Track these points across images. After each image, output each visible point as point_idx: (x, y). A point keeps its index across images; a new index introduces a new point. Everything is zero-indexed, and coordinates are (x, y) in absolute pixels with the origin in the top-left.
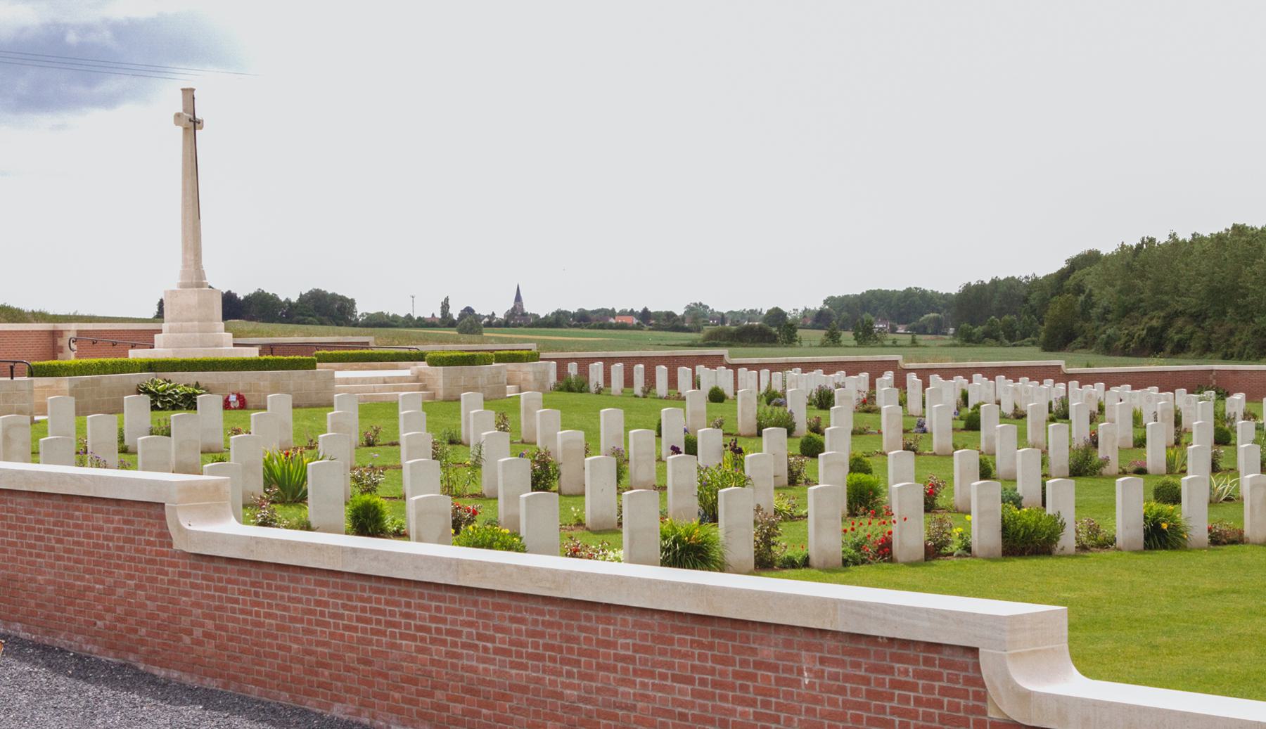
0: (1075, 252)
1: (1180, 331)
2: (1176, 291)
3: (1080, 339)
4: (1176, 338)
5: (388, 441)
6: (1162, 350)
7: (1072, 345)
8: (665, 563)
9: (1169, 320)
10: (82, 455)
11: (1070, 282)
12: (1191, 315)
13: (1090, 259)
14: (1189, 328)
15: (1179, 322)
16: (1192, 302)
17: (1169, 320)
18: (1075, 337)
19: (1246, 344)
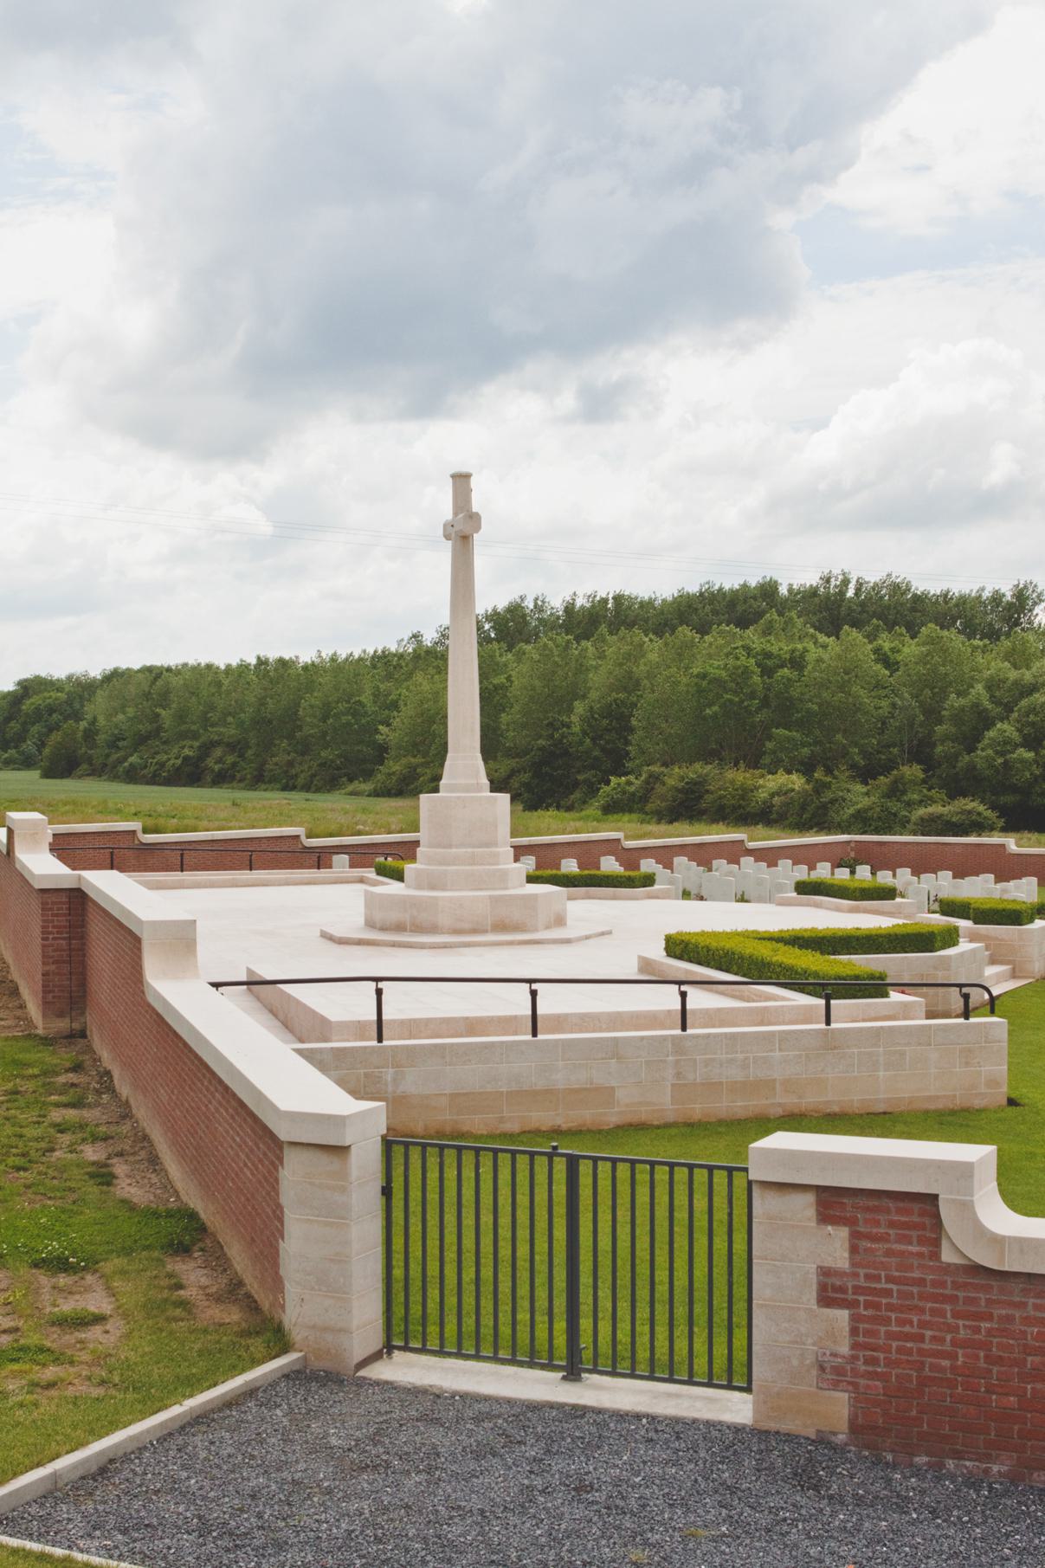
0: (27, 674)
1: (220, 760)
2: (205, 721)
3: (85, 766)
4: (217, 767)
5: (443, 557)
6: (199, 779)
7: (78, 772)
8: (928, 1018)
9: (206, 749)
10: (126, 1114)
11: (27, 706)
12: (228, 745)
13: (185, 665)
14: (230, 759)
15: (218, 752)
16: (230, 732)
17: (206, 749)
18: (78, 765)
19: (313, 776)
